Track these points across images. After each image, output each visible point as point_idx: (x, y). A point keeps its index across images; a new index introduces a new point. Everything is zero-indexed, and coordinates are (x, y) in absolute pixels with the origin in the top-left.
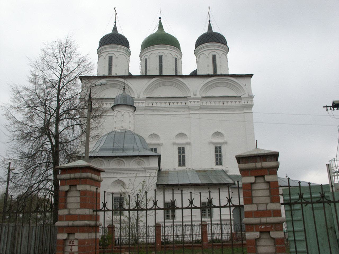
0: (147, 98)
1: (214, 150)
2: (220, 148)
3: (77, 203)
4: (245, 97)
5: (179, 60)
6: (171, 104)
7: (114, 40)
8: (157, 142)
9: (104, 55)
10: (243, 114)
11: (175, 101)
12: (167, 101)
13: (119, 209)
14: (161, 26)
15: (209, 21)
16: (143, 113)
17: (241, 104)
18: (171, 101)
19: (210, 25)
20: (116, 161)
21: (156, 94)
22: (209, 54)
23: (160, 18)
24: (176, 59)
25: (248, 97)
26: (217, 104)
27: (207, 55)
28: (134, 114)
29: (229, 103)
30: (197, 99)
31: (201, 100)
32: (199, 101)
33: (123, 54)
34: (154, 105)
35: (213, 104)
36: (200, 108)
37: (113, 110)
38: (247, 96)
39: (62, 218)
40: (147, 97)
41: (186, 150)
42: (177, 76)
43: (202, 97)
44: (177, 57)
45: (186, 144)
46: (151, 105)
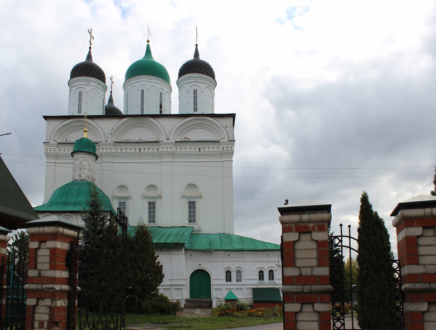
0: (115, 142)
1: (187, 205)
2: (154, 203)
3: (40, 263)
4: (224, 142)
5: (165, 94)
6: (142, 150)
7: (87, 70)
8: (155, 195)
9: (74, 89)
11: (146, 146)
12: (138, 147)
13: (341, 280)
14: (148, 51)
15: (197, 45)
16: (54, 161)
18: (202, 146)
20: (65, 217)
21: (125, 138)
22: (189, 88)
23: (148, 41)
24: (161, 94)
27: (188, 89)
28: (96, 162)
30: (171, 144)
32: (173, 146)
33: (95, 88)
34: (124, 151)
36: (173, 155)
37: (73, 156)
38: (227, 141)
39: (32, 280)
40: (117, 141)
41: (197, 205)
42: (161, 116)
43: (176, 142)
45: (156, 198)
46: (120, 152)
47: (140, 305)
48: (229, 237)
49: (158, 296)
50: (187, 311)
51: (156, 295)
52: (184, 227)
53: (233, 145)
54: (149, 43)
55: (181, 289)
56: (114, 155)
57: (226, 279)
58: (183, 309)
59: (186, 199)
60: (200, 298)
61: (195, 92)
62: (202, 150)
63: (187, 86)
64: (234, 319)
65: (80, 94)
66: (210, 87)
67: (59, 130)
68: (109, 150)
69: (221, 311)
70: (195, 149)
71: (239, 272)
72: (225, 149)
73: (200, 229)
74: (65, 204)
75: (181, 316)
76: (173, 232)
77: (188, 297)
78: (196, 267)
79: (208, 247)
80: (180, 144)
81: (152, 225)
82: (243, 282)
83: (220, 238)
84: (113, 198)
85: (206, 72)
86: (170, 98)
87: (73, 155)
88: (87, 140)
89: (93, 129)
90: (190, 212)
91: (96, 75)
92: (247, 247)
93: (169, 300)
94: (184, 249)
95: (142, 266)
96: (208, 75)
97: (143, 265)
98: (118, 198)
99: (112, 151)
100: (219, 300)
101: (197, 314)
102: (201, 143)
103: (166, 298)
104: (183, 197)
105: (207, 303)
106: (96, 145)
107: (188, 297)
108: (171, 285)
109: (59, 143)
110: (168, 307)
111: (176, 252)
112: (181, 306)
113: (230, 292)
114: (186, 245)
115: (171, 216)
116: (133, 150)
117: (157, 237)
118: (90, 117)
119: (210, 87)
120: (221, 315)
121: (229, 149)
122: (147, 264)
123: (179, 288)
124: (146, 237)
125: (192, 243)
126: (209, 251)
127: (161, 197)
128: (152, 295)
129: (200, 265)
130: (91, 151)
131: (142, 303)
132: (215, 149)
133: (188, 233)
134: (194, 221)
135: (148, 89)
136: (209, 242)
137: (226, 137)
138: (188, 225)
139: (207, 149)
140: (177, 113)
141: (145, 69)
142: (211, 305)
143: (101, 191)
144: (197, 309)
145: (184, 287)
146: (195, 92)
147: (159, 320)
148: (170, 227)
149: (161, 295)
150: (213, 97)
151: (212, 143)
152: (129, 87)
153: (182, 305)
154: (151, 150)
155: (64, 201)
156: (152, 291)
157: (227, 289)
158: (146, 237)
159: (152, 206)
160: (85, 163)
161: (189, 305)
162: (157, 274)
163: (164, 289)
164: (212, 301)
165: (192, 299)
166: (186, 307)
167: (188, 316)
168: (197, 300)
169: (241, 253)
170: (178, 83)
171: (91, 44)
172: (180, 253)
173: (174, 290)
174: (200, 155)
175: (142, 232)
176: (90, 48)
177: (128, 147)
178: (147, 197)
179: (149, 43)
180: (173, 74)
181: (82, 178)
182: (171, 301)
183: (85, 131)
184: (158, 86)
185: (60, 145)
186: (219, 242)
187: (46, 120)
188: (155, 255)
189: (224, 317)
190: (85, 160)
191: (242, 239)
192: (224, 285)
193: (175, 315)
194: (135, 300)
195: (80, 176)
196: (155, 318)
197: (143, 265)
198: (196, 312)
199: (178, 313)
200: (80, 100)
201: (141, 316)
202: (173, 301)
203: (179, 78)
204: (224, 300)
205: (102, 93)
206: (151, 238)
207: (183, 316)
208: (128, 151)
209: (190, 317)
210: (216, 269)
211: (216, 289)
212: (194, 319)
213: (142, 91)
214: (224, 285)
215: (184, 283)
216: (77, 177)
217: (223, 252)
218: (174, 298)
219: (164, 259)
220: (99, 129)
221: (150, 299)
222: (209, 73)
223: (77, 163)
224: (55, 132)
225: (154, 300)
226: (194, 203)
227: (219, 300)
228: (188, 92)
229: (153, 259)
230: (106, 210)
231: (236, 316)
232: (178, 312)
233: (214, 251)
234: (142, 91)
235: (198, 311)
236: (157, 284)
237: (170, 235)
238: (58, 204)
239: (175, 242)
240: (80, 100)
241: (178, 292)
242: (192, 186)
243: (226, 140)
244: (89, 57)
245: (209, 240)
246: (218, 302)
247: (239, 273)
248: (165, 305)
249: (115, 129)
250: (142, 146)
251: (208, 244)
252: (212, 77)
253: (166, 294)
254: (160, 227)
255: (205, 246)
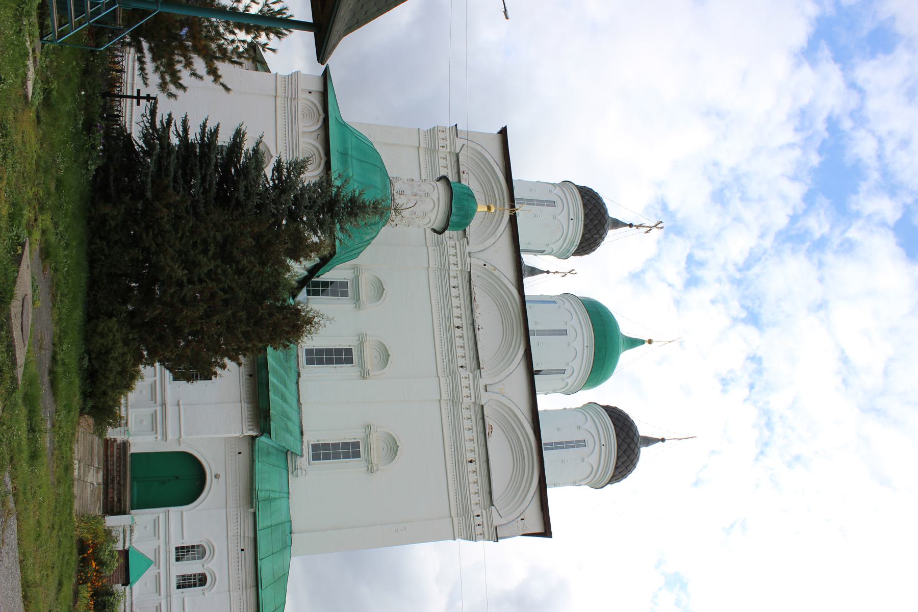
0: (470, 273)
5: (563, 380)
6: (458, 332)
8: (368, 365)
9: (558, 191)
10: (447, 513)
11: (467, 341)
12: (465, 322)
15: (663, 440)
16: (422, 145)
17: (474, 507)
18: (479, 466)
19: (656, 441)
23: (650, 342)
24: (563, 372)
25: (492, 524)
26: (473, 488)
28: (429, 232)
29: (459, 342)
30: (477, 395)
31: (475, 403)
34: (454, 292)
35: (473, 488)
36: (455, 402)
38: (495, 524)
42: (531, 373)
43: (482, 406)
44: (567, 373)
46: (452, 285)
47: (110, 316)
48: (286, 546)
49: (135, 365)
50: (96, 447)
51: (139, 359)
52: (302, 433)
53: (487, 537)
54: (647, 344)
55: (154, 429)
56: (443, 270)
57: (183, 548)
58: (100, 435)
59: (363, 435)
60: (133, 479)
61: (582, 444)
62: (471, 467)
63: (589, 425)
64: (68, 589)
65: (552, 204)
66: (592, 475)
67: (483, 157)
68: (452, 260)
69: (95, 545)
70: (472, 451)
71: (202, 580)
72: (478, 520)
73: (299, 471)
74: (344, 155)
75: (81, 430)
76: (291, 407)
77: (133, 450)
78: (211, 466)
79: (261, 495)
80: (479, 415)
81: (303, 358)
82: (177, 594)
83: (282, 523)
84: (355, 268)
85: (620, 463)
86: (554, 391)
87: (442, 181)
88: (474, 211)
89: (490, 228)
90: (336, 456)
91: (587, 236)
92: (265, 594)
93: (126, 396)
94: (254, 434)
95: (216, 318)
96: (616, 468)
97: (218, 324)
98: (357, 279)
99: (452, 267)
100: (128, 532)
101: (85, 475)
102: (485, 464)
103: (129, 387)
104: (368, 428)
105: (119, 500)
106: (460, 232)
107: (133, 450)
108: (163, 404)
109: (457, 155)
110: (105, 393)
111: (246, 414)
112: (110, 429)
113: (149, 563)
114: (263, 439)
115: (322, 402)
116: (456, 312)
117: (278, 368)
118: (513, 220)
119: (592, 475)
120: (82, 546)
121: (479, 530)
122: (220, 335)
123: (157, 424)
124: (288, 333)
125: (269, 453)
126: (252, 499)
127: (364, 378)
128: (138, 348)
129: (217, 476)
130: (453, 218)
131: (115, 319)
132: (476, 498)
133: (291, 443)
134: (316, 457)
135: (569, 345)
136: (272, 495)
137: (503, 521)
138: (305, 444)
139: (474, 477)
140: (541, 407)
141: (605, 339)
142: (112, 513)
143: (373, 238)
144: (101, 474)
145: (159, 438)
146: (582, 444)
147: (64, 364)
148: (299, 400)
149: (138, 372)
150: (574, 484)
151: (488, 490)
152: (567, 305)
153: (112, 433)
154: (460, 352)
155: (350, 153)
156: (147, 349)
157: (157, 551)
158: (288, 333)
159: (341, 356)
160: (427, 205)
161: (112, 452)
162: (194, 367)
163: (153, 387)
164: (124, 513)
165: (129, 459)
166: (108, 444)
167: (79, 450)
168: (125, 473)
169: (251, 581)
170: (591, 405)
171: (637, 227)
172: (245, 423)
173: (152, 410)
174: (458, 463)
175: (294, 325)
176: (548, 272)
177: (463, 301)
178: (361, 344)
179: (647, 344)
180: (607, 393)
181: (397, 197)
182: (123, 401)
183: (489, 208)
184: (576, 364)
185: (454, 159)
186: (274, 523)
187: (500, 132)
188: (241, 357)
189: (75, 558)
190: (432, 205)
191: (282, 578)
192: (167, 543)
193: (82, 413)
194: (125, 303)
195: (402, 193)
196: (71, 353)
197: (218, 324)
198: (93, 471)
199: (88, 421)
200: (540, 203)
201: (78, 315)
202: (123, 409)
203: (603, 407)
204: (127, 547)
205: (556, 247)
206: (286, 346)
207: (80, 434)
208: (455, 302)
209: (76, 456)
210: (207, 522)
211: (156, 522)
212: (68, 468)
213: (564, 332)
214: (167, 543)
215: (170, 436)
216: (398, 186)
217: (251, 535)
218: (130, 411)
219: (231, 377)
220: (492, 240)
221: (126, 343)
222: (620, 470)
223: (427, 188)
224: (479, 149)
225: (124, 354)
226: (357, 455)
227: (128, 532)
228: (579, 428)
229: (233, 349)
230: (337, 243)
231: (76, 593)
232: (91, 421)
233: (252, 510)
234: (564, 332)
235: (95, 478)
236: (168, 360)
237: (284, 400)
238: (344, 141)
239: (272, 412)
240: (540, 203)
241: (147, 422)
242: (393, 448)
243: (497, 521)
244: (617, 224)
245: (277, 495)
246: (121, 530)
247: (200, 580)
248: (110, 383)
249: (496, 273)
250: (466, 331)
251: (268, 494)
252: (613, 477)
253: (141, 387)
254: (299, 375)
255: (263, 487)
